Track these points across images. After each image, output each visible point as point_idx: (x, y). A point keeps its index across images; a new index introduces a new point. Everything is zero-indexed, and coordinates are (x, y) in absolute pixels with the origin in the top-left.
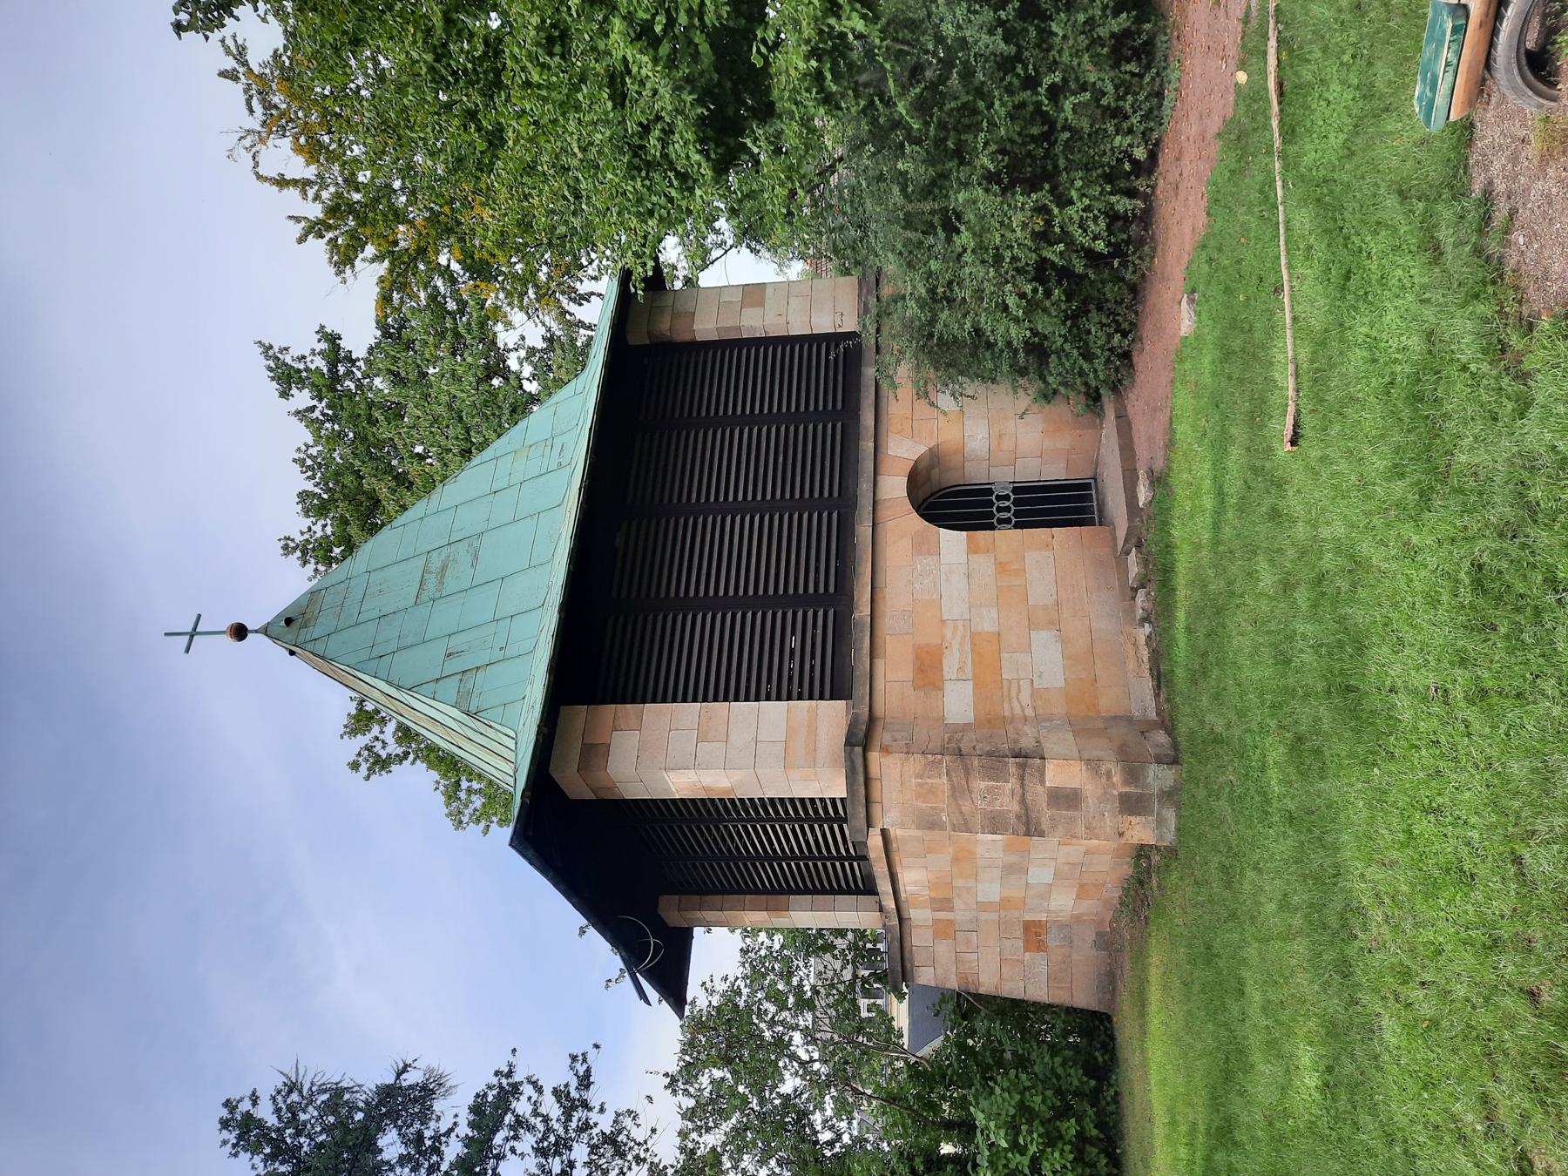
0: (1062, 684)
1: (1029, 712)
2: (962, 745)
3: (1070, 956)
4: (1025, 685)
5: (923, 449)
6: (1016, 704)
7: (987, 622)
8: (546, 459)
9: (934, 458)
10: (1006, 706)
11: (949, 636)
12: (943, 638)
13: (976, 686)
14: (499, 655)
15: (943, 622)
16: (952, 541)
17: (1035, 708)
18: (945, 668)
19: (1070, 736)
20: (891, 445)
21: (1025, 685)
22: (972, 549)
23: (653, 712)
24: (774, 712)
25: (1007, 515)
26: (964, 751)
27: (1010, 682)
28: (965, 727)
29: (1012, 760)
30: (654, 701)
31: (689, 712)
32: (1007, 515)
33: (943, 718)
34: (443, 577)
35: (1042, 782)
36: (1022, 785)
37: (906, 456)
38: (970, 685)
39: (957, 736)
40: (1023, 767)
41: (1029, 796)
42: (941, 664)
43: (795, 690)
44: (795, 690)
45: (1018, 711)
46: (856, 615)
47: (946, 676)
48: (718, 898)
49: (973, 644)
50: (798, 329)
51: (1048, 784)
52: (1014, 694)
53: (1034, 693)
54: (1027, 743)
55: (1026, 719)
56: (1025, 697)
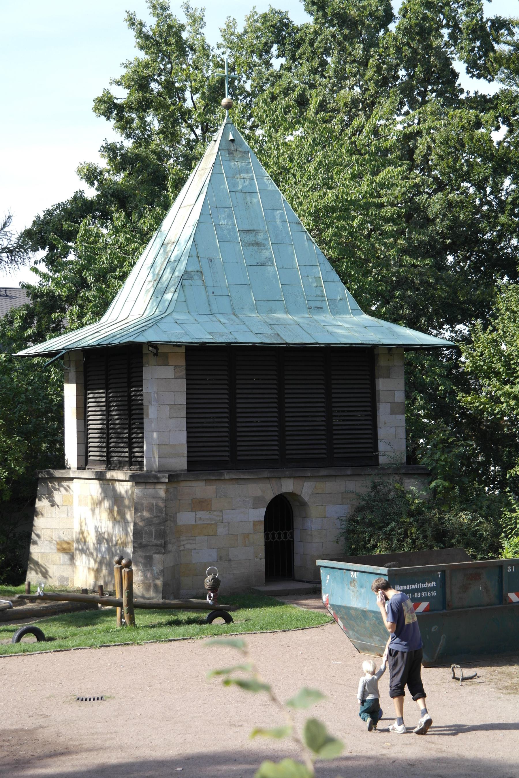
0: (194, 562)
1: (182, 548)
2: (169, 521)
3: (55, 564)
4: (194, 546)
5: (306, 499)
6: (185, 542)
7: (221, 530)
8: (314, 298)
9: (304, 504)
10: (184, 538)
11: (215, 513)
12: (215, 511)
13: (192, 525)
14: (210, 290)
15: (222, 511)
16: (260, 514)
17: (183, 550)
18: (201, 512)
19: (172, 564)
20: (309, 484)
21: (194, 546)
22: (255, 523)
23: (182, 383)
24: (182, 438)
25: (282, 538)
26: (166, 523)
27: (195, 540)
28: (175, 522)
29: (163, 541)
30: (187, 384)
31: (182, 400)
32: (282, 538)
33: (179, 512)
34: (253, 245)
35: (155, 553)
36: (153, 546)
37: (303, 491)
38: (194, 523)
39: (172, 519)
40: (161, 546)
41: (149, 547)
42: (203, 510)
43: (192, 449)
44: (192, 449)
45: (182, 543)
46: (225, 472)
47: (197, 513)
48: (82, 381)
49: (211, 524)
50: (381, 433)
51: (154, 555)
52: (190, 541)
53: (190, 550)
54: (170, 547)
55: (179, 546)
56: (188, 546)
